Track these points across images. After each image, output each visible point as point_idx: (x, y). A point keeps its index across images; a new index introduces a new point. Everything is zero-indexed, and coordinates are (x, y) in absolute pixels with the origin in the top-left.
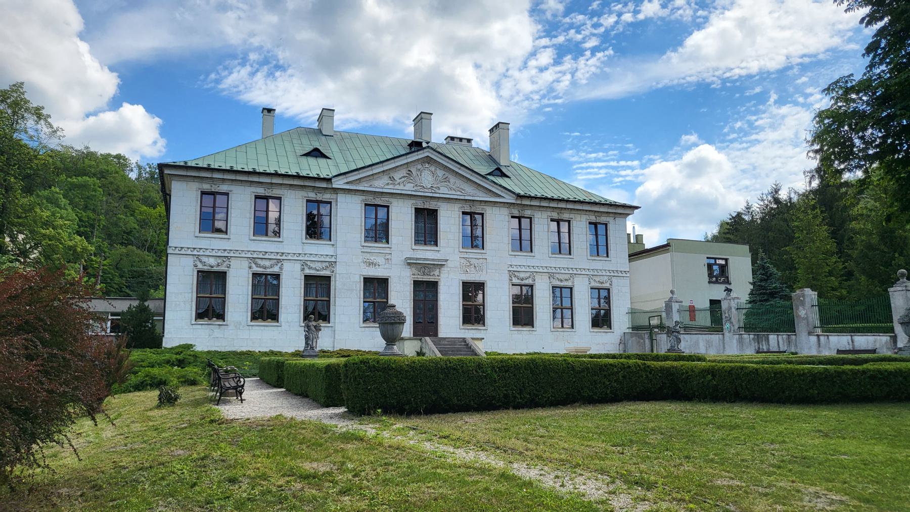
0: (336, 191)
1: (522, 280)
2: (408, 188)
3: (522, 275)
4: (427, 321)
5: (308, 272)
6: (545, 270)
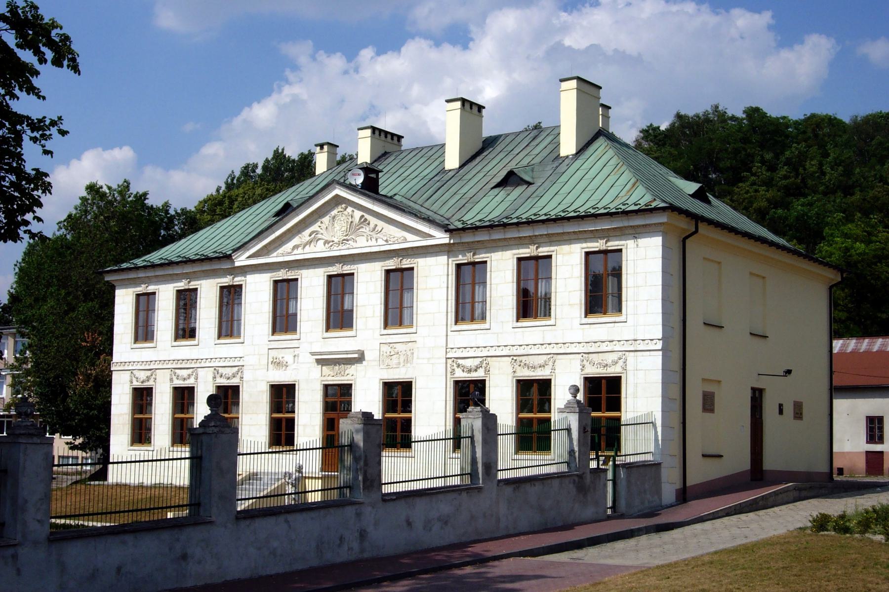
2: (318, 250)
5: (461, 375)
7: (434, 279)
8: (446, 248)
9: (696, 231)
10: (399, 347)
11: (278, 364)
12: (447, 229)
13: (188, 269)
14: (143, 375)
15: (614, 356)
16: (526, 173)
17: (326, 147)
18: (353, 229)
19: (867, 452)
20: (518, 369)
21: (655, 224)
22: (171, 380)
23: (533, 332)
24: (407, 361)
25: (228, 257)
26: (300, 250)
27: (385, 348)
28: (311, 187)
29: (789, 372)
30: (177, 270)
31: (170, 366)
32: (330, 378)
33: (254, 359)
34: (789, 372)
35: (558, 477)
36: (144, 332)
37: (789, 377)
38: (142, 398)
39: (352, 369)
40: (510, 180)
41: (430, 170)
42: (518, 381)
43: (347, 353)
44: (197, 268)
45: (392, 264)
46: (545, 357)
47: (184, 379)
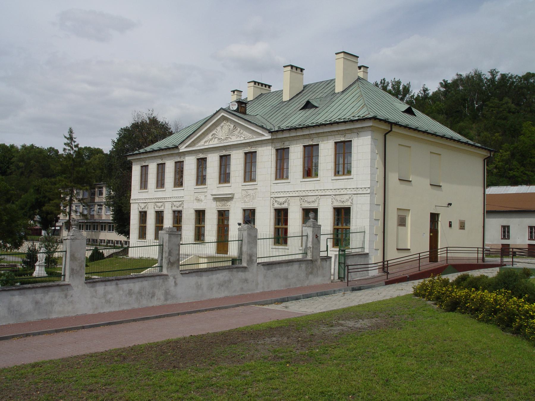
0: (184, 154)
2: (215, 143)
3: (311, 199)
5: (277, 206)
7: (266, 157)
8: (271, 141)
9: (391, 131)
11: (198, 200)
12: (270, 132)
13: (161, 153)
14: (143, 206)
15: (347, 197)
16: (316, 102)
17: (236, 92)
18: (231, 132)
19: (529, 245)
20: (303, 203)
21: (367, 127)
22: (154, 208)
23: (310, 184)
24: (253, 199)
25: (176, 147)
26: (207, 144)
27: (244, 192)
28: (286, 112)
29: (450, 204)
30: (156, 154)
31: (154, 201)
32: (220, 207)
33: (191, 197)
34: (450, 204)
35: (298, 261)
36: (144, 185)
37: (450, 207)
38: (143, 215)
39: (229, 203)
40: (308, 105)
41: (276, 103)
42: (334, 208)
43: (226, 194)
44: (165, 153)
46: (315, 197)
47: (159, 207)
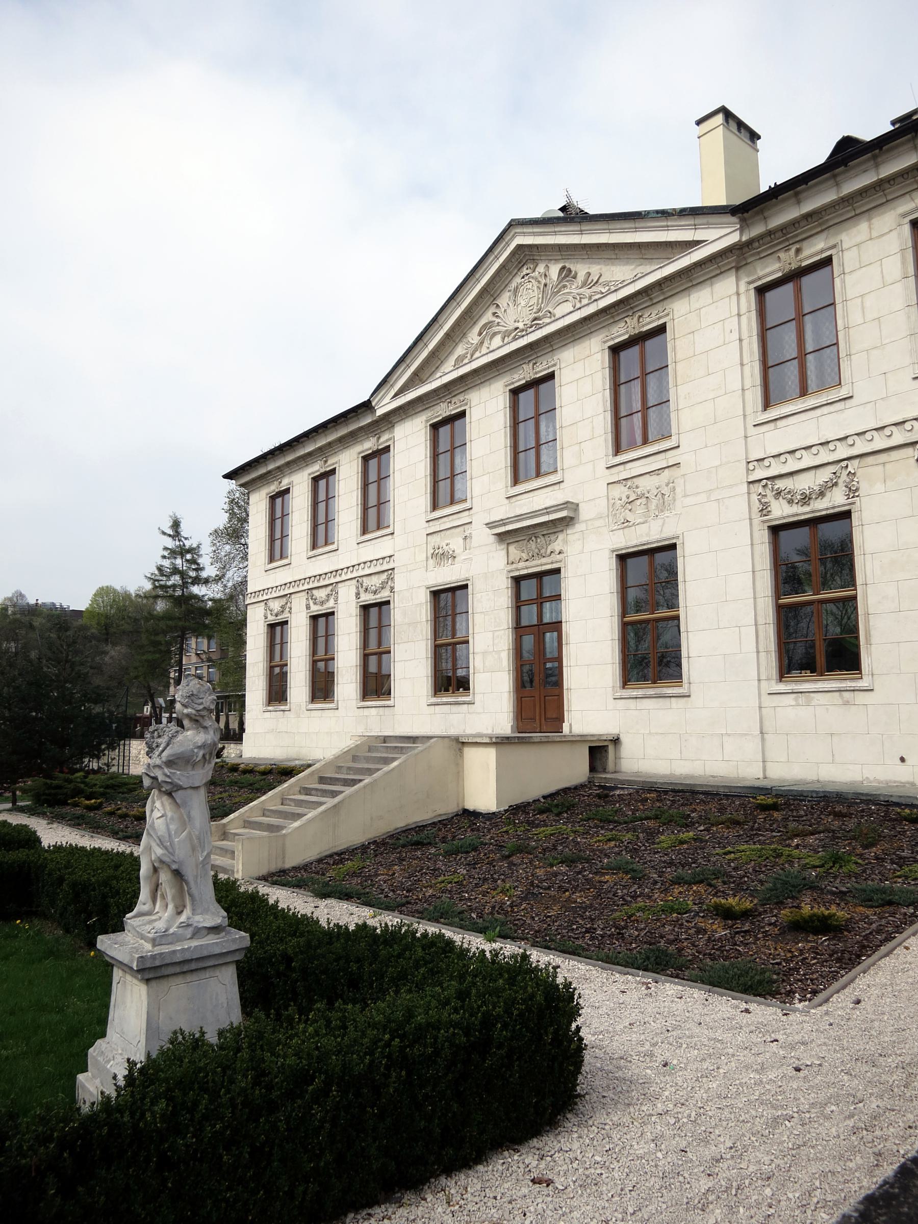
1: (806, 499)
4: (539, 683)
5: (782, 511)
6: (899, 438)
10: (645, 484)
45: (620, 332)
